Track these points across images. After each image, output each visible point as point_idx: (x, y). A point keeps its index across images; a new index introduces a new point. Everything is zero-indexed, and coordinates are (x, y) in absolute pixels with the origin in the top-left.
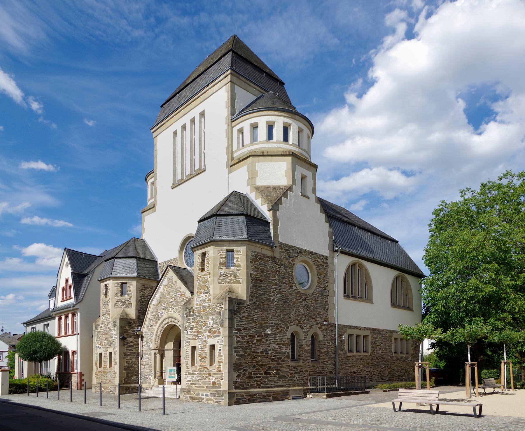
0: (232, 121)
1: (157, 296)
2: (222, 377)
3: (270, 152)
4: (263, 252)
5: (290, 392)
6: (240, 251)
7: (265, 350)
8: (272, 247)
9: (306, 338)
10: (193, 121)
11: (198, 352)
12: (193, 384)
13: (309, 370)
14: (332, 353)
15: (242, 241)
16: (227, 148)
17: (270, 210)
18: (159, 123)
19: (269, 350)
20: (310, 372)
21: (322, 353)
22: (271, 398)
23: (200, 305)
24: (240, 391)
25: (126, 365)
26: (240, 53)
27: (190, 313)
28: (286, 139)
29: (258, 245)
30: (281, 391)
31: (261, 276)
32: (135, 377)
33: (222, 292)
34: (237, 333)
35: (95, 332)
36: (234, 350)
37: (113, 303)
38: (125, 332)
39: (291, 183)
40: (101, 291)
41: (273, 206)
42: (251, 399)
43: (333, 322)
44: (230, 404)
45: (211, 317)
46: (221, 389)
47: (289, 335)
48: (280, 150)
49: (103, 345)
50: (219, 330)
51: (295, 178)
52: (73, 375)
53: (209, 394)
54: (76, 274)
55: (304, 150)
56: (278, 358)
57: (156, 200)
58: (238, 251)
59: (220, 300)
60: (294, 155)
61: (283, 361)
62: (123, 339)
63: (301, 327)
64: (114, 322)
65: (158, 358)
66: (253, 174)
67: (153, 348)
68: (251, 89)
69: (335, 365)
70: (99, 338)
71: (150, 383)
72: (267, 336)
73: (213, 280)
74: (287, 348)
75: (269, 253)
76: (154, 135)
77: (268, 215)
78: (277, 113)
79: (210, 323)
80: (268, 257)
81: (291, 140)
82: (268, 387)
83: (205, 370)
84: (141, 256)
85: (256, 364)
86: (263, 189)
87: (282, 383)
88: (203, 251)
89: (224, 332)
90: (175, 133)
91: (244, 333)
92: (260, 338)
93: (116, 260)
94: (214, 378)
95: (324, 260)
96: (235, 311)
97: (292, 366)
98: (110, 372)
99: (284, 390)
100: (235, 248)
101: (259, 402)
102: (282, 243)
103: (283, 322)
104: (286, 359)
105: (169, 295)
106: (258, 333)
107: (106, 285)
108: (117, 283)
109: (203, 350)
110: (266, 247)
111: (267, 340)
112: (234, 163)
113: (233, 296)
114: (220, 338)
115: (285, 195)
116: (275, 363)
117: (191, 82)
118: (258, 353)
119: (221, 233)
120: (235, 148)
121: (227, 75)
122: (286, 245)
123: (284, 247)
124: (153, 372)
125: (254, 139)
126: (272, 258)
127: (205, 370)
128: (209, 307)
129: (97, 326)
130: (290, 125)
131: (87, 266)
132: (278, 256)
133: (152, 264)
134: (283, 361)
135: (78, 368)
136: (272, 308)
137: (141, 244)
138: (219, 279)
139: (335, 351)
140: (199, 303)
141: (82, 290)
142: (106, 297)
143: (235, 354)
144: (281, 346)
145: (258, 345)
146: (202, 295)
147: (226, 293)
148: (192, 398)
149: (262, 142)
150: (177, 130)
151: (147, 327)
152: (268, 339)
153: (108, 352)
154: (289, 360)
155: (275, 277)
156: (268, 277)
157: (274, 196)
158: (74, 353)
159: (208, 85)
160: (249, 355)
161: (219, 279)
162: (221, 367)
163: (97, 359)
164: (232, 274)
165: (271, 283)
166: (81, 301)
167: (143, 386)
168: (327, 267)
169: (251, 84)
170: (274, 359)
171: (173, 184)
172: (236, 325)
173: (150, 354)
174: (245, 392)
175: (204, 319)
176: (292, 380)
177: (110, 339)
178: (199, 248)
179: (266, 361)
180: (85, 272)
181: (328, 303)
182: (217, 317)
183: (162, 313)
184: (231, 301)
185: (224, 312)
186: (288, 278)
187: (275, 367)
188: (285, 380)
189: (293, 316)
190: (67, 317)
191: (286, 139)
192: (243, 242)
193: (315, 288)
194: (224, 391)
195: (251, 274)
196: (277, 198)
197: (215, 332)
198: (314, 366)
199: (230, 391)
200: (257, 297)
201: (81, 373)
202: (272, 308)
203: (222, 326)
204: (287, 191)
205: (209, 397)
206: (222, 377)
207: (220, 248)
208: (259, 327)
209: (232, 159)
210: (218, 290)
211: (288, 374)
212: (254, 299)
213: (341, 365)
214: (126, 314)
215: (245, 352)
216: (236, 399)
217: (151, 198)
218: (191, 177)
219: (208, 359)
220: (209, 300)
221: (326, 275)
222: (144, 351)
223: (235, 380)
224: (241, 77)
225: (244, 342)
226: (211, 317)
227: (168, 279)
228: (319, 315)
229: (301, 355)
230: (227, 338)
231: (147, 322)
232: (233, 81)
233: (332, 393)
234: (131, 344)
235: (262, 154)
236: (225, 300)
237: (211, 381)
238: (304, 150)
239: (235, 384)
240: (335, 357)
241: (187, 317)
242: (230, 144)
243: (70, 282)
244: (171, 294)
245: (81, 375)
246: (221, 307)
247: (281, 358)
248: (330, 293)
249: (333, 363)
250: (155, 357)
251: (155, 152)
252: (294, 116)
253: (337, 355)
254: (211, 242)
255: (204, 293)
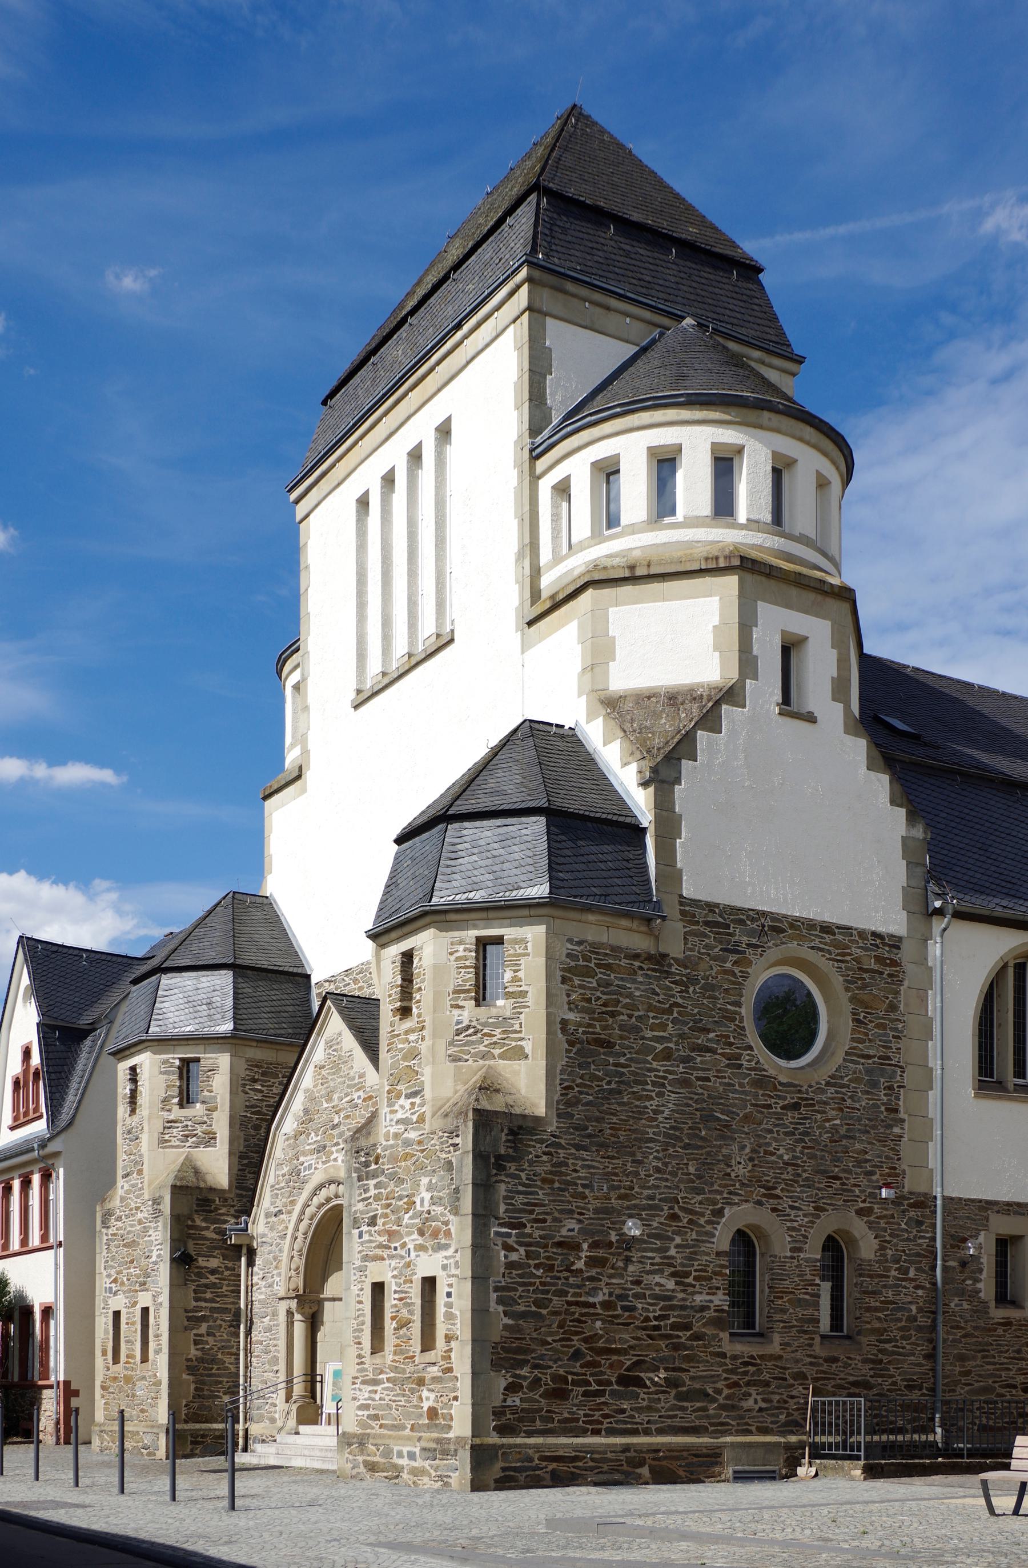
0: (535, 456)
1: (296, 1104)
2: (455, 1390)
3: (660, 563)
4: (614, 942)
5: (727, 1455)
6: (523, 941)
7: (620, 1297)
8: (649, 920)
9: (799, 1250)
10: (415, 456)
11: (390, 1301)
12: (376, 1417)
13: (811, 1372)
14: (920, 1310)
15: (529, 906)
16: (520, 557)
17: (645, 784)
18: (312, 466)
19: (637, 1296)
20: (815, 1380)
21: (869, 1309)
22: (645, 1471)
23: (396, 1136)
24: (518, 1440)
25: (193, 1352)
26: (571, 192)
27: (367, 1164)
28: (723, 505)
29: (591, 917)
30: (686, 1448)
31: (604, 1028)
32: (226, 1399)
33: (462, 1089)
34: (509, 1235)
35: (104, 1236)
36: (494, 1296)
37: (156, 1133)
38: (189, 1236)
39: (734, 674)
40: (120, 1090)
41: (654, 770)
42: (563, 1473)
43: (922, 1189)
44: (477, 1486)
45: (425, 1181)
46: (451, 1435)
47: (722, 1238)
48: (701, 551)
49: (122, 1284)
50: (446, 1223)
51: (755, 651)
52: (47, 1393)
53: (417, 1450)
54: (53, 1028)
55: (803, 540)
56: (674, 1327)
57: (306, 752)
58: (516, 941)
59: (449, 1119)
60: (747, 566)
61: (697, 1337)
62: (183, 1261)
63: (774, 1210)
64: (156, 1201)
65: (299, 1329)
66: (599, 653)
67: (282, 1294)
68: (613, 321)
69: (931, 1356)
70: (113, 1258)
71: (273, 1421)
72: (628, 1243)
73: (433, 1048)
74: (713, 1291)
75: (639, 942)
76: (301, 510)
77: (641, 802)
78: (685, 414)
79: (422, 1200)
80: (636, 956)
81: (742, 515)
82: (634, 1432)
83: (409, 1369)
84: (251, 958)
85: (583, 1347)
86: (629, 705)
87: (692, 1419)
88: (405, 945)
89: (461, 1230)
90: (363, 502)
91: (537, 1234)
92: (601, 1253)
93: (167, 980)
94: (432, 1396)
95: (885, 952)
96: (499, 1157)
97: (734, 1357)
98: (144, 1378)
99: (700, 1446)
100: (508, 933)
101: (596, 1484)
102: (695, 903)
103: (699, 1191)
104: (709, 1331)
105: (329, 1099)
106: (592, 1234)
107: (133, 1069)
108: (166, 1061)
109: (403, 1301)
110: (624, 923)
111: (628, 1260)
112: (543, 608)
113: (497, 1104)
114: (450, 1252)
115: (710, 720)
116: (662, 1344)
117: (413, 312)
118: (593, 1305)
119: (458, 881)
120: (545, 555)
121: (518, 287)
122: (711, 907)
123: (700, 915)
124: (282, 1377)
125: (609, 518)
126: (650, 958)
127: (409, 1369)
128: (420, 1143)
129: (108, 1214)
130: (740, 450)
131: (96, 995)
132: (674, 947)
133: (289, 987)
134: (697, 1337)
135: (59, 1368)
136: (651, 1140)
137: (258, 915)
138: (451, 1043)
139: (933, 1300)
140: (392, 1130)
141: (74, 1085)
142: (133, 1111)
143: (501, 1308)
144: (690, 1280)
145: (591, 1279)
146: (402, 1101)
147: (470, 1094)
148: (372, 1467)
149: (633, 529)
150: (367, 493)
151: (268, 1215)
152: (635, 1255)
153: (138, 1307)
154: (725, 1335)
155: (663, 1027)
156: (638, 1030)
157: (667, 727)
158: (47, 1312)
159: (458, 326)
160: (556, 1313)
161: (451, 1043)
162: (453, 1355)
163: (106, 1332)
164: (495, 1026)
165: (647, 1050)
166: (70, 1124)
167: (255, 1429)
168: (896, 979)
169: (614, 303)
170: (657, 1328)
171: (359, 692)
172: (502, 1208)
173: (275, 1314)
174: (537, 1447)
175: (406, 1188)
176: (733, 1407)
177: (144, 1262)
178: (394, 935)
179: (625, 1337)
180: (85, 1021)
181: (902, 1115)
182: (442, 1178)
183: (310, 1166)
184: (484, 1121)
185: (461, 1161)
186: (721, 1030)
187: (662, 1360)
188: (704, 1409)
189: (741, 1170)
190: (26, 1184)
191: (723, 505)
192: (533, 912)
193: (839, 1059)
194: (459, 1440)
195: (564, 1022)
196: (677, 732)
197: (435, 1234)
198: (835, 1360)
199: (477, 1441)
200: (588, 1104)
201: (67, 1383)
202: (651, 1140)
203: (456, 1211)
204: (718, 703)
205: (418, 1463)
206: (455, 1390)
207: (457, 934)
208: (597, 1211)
209: (535, 594)
210: (450, 1083)
211: (720, 1385)
212: (579, 1113)
213: (962, 1358)
214: (197, 1172)
215: (537, 1303)
216: (496, 1469)
217: (293, 745)
218: (414, 663)
219: (416, 1328)
220: (421, 1119)
221: (893, 1008)
222: (256, 1305)
223: (497, 1404)
224: (570, 286)
225: (537, 1267)
226: (425, 1181)
227: (329, 1044)
228: (859, 1163)
229: (777, 1317)
230: (468, 1253)
231: (266, 1201)
232: (537, 305)
233: (889, 1462)
234: (212, 1279)
235: (627, 574)
236: (465, 1121)
237: (426, 1405)
238: (803, 540)
239: (496, 1417)
240: (933, 1328)
241: (360, 1179)
242: (527, 540)
243: (36, 1060)
244: (335, 1096)
245: (69, 1391)
246: (455, 1145)
247: (687, 1327)
248: (910, 1078)
249: (924, 1348)
250: (290, 1324)
251: (303, 574)
252: (752, 415)
253: (940, 1318)
254: (424, 914)
255: (408, 1096)
